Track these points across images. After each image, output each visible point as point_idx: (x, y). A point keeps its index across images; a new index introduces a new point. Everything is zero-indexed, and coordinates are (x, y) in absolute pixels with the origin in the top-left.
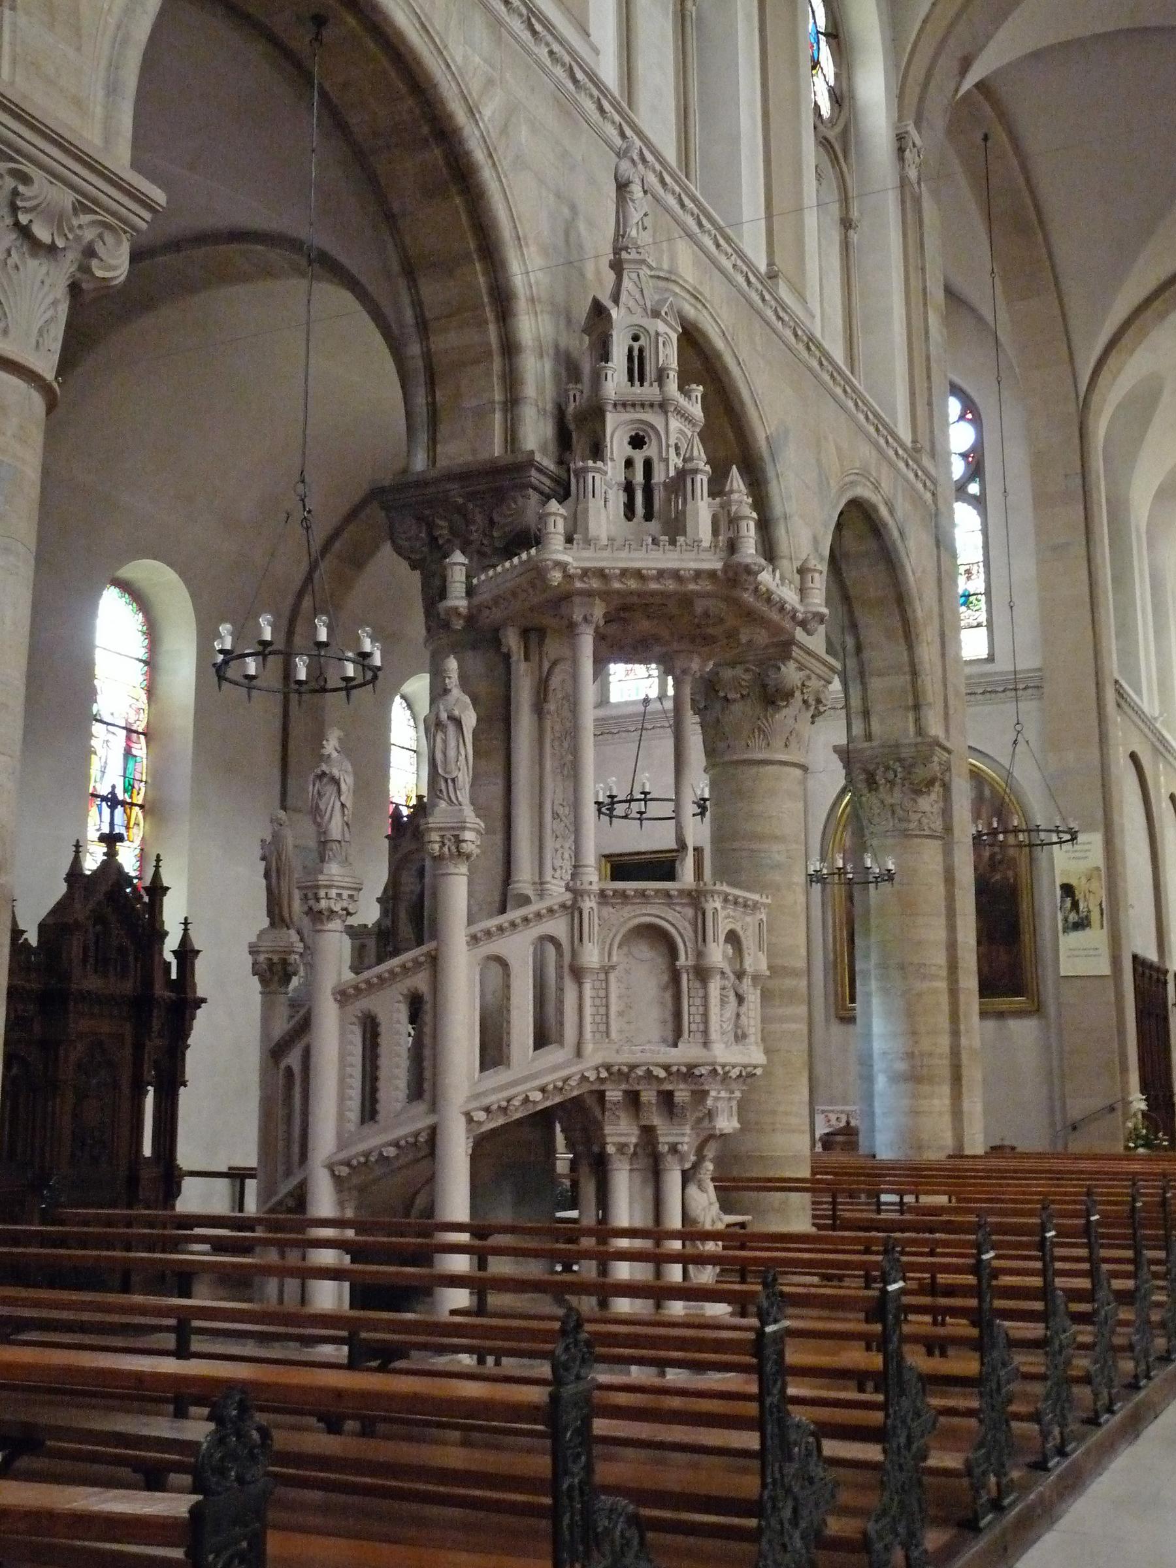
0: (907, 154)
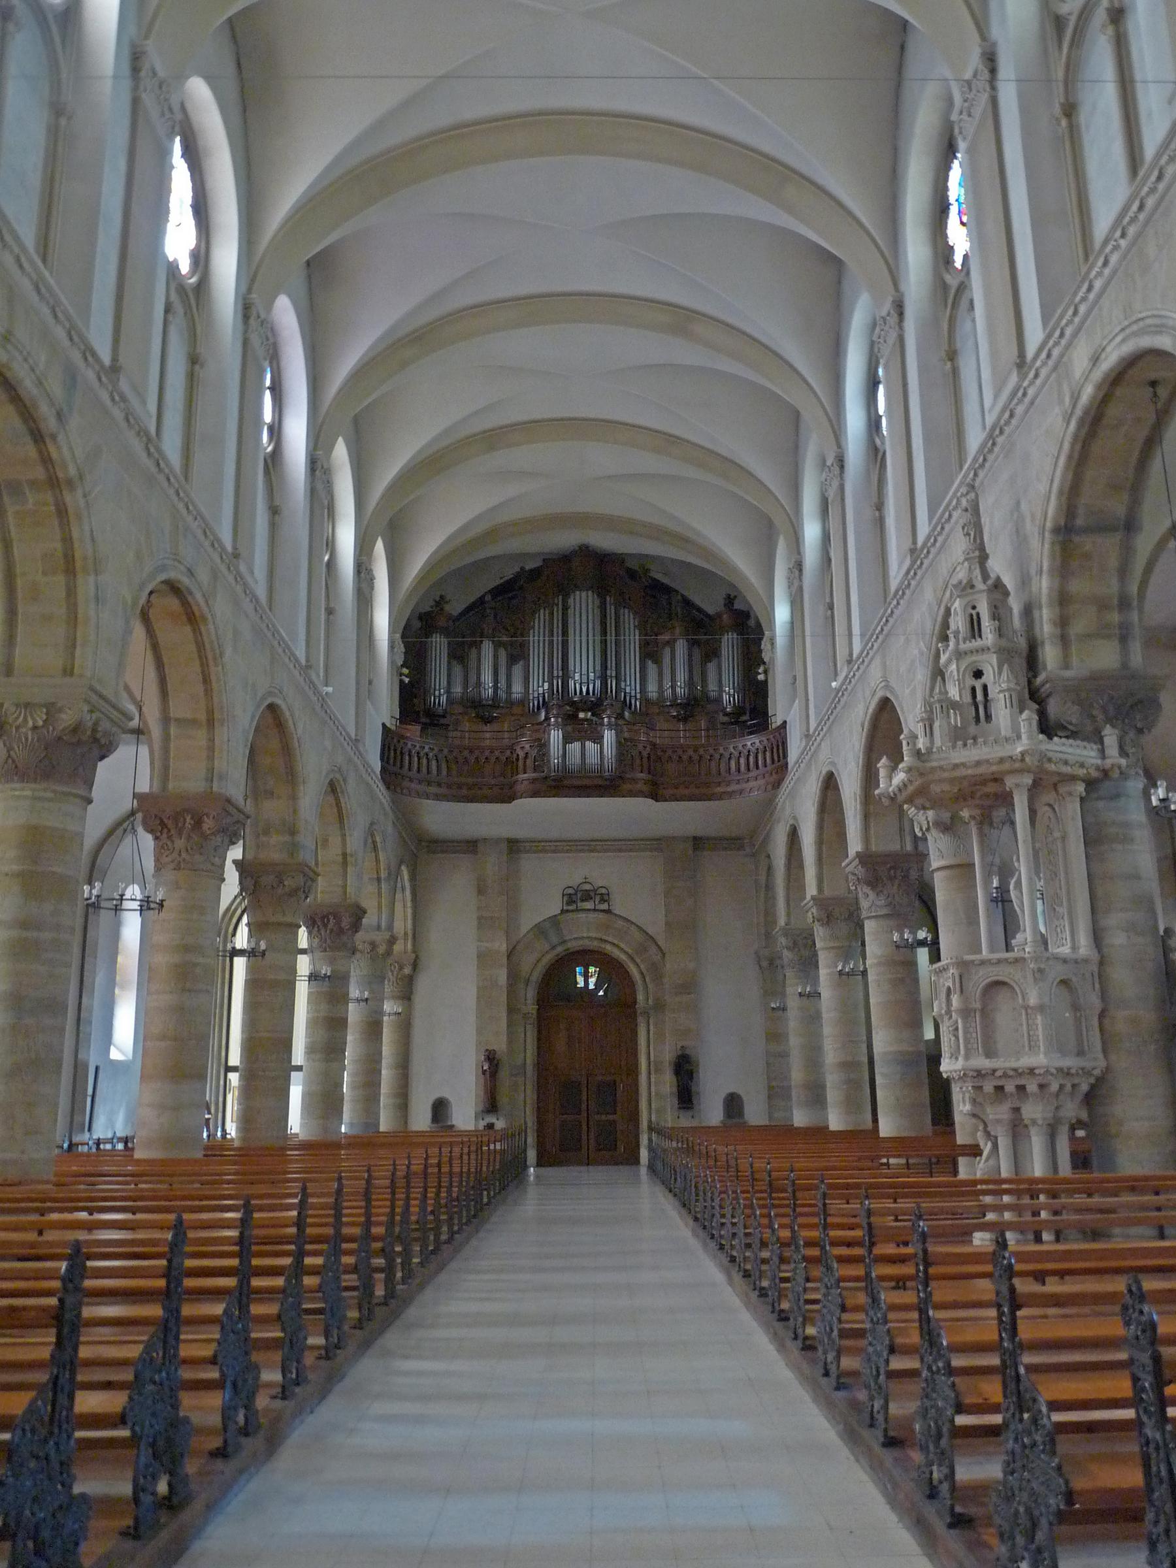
0: (252, 321)
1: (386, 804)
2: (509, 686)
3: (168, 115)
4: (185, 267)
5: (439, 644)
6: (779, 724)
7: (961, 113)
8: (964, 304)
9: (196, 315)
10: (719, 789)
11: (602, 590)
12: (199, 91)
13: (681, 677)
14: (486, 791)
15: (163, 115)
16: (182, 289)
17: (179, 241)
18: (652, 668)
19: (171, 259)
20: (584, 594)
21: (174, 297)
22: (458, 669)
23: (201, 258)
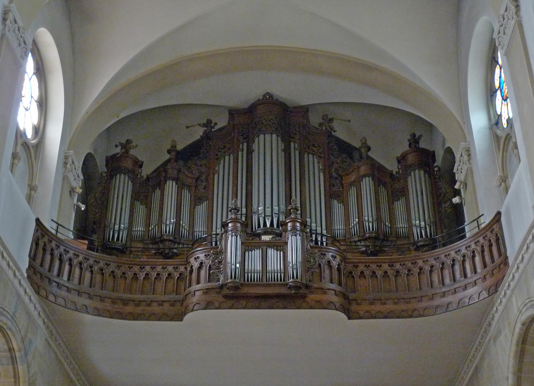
1: (35, 314)
2: (192, 224)
3: (23, 45)
4: (29, 134)
5: (123, 186)
6: (486, 220)
7: (499, 33)
8: (511, 145)
9: (34, 162)
10: (424, 304)
11: (287, 138)
12: (46, 38)
13: (369, 215)
14: (156, 308)
15: (20, 45)
16: (26, 145)
17: (27, 119)
18: (337, 207)
19: (22, 128)
20: (268, 137)
21: (20, 149)
22: (141, 209)
23: (40, 131)
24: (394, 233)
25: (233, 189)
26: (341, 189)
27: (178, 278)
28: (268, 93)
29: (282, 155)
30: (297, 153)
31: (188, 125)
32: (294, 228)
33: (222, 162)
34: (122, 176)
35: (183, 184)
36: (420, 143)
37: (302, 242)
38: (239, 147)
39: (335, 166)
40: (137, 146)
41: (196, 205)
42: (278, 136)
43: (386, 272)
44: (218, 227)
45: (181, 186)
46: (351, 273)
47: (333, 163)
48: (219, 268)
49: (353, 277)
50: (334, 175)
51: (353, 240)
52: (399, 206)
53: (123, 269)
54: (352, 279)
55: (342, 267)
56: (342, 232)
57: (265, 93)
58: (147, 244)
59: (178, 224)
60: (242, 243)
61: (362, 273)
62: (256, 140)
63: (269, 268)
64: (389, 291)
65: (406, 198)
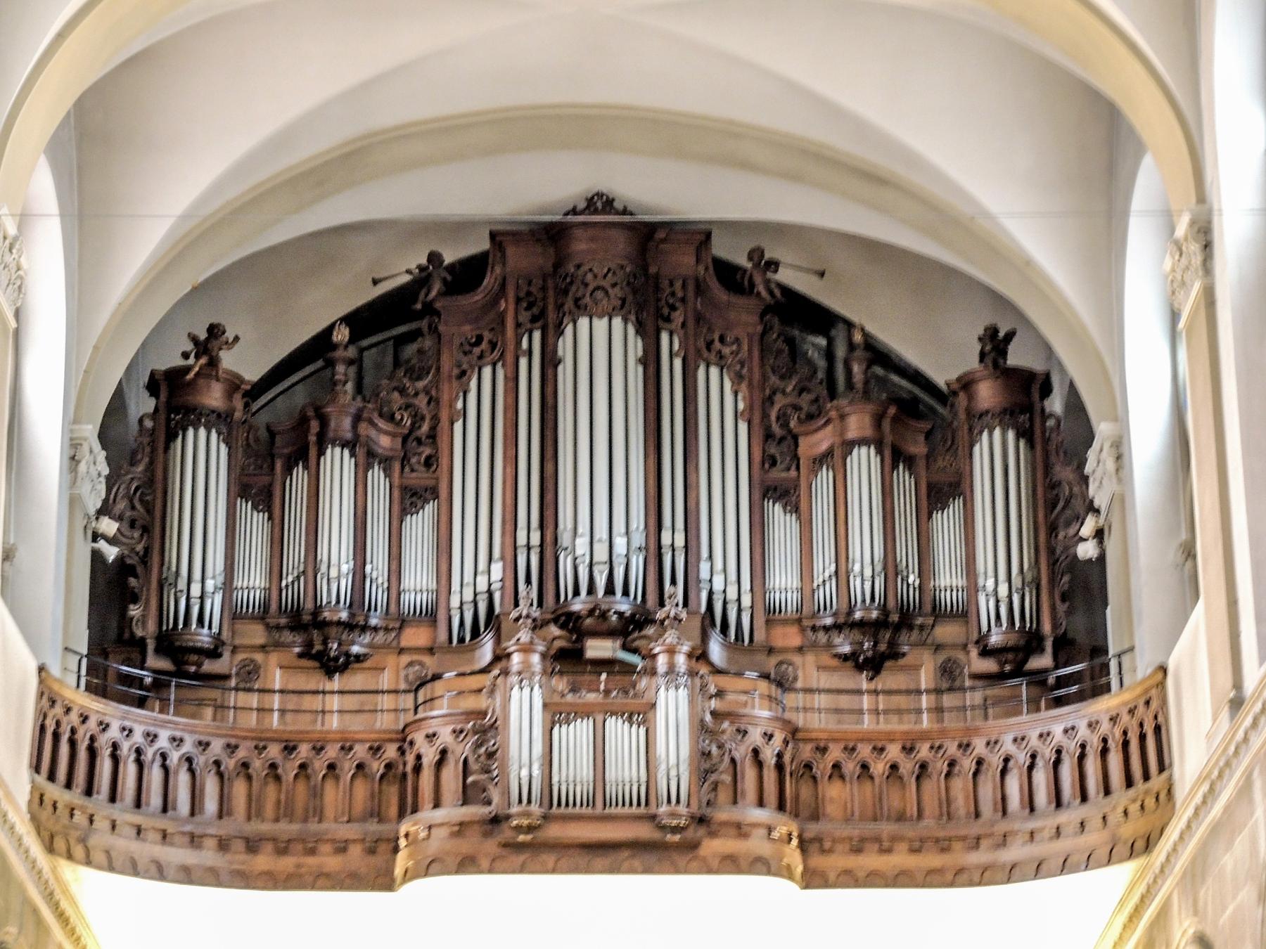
5: (204, 461)
13: (865, 548)
20: (601, 325)
22: (255, 524)
24: (928, 607)
25: (505, 468)
26: (793, 473)
27: (382, 777)
28: (600, 195)
29: (636, 374)
30: (678, 363)
31: (377, 276)
32: (671, 669)
33: (473, 384)
34: (202, 432)
35: (371, 454)
36: (1009, 357)
37: (692, 702)
38: (519, 343)
39: (780, 401)
40: (237, 339)
41: (404, 512)
42: (625, 320)
43: (894, 767)
44: (465, 581)
45: (368, 458)
46: (808, 766)
47: (774, 393)
48: (487, 771)
49: (814, 778)
50: (777, 430)
51: (819, 623)
52: (946, 524)
53: (241, 754)
54: (810, 783)
55: (787, 758)
56: (793, 598)
57: (595, 191)
58: (278, 628)
59: (359, 576)
60: (545, 705)
61: (837, 766)
62: (569, 330)
63: (611, 775)
64: (901, 817)
65: (965, 501)
